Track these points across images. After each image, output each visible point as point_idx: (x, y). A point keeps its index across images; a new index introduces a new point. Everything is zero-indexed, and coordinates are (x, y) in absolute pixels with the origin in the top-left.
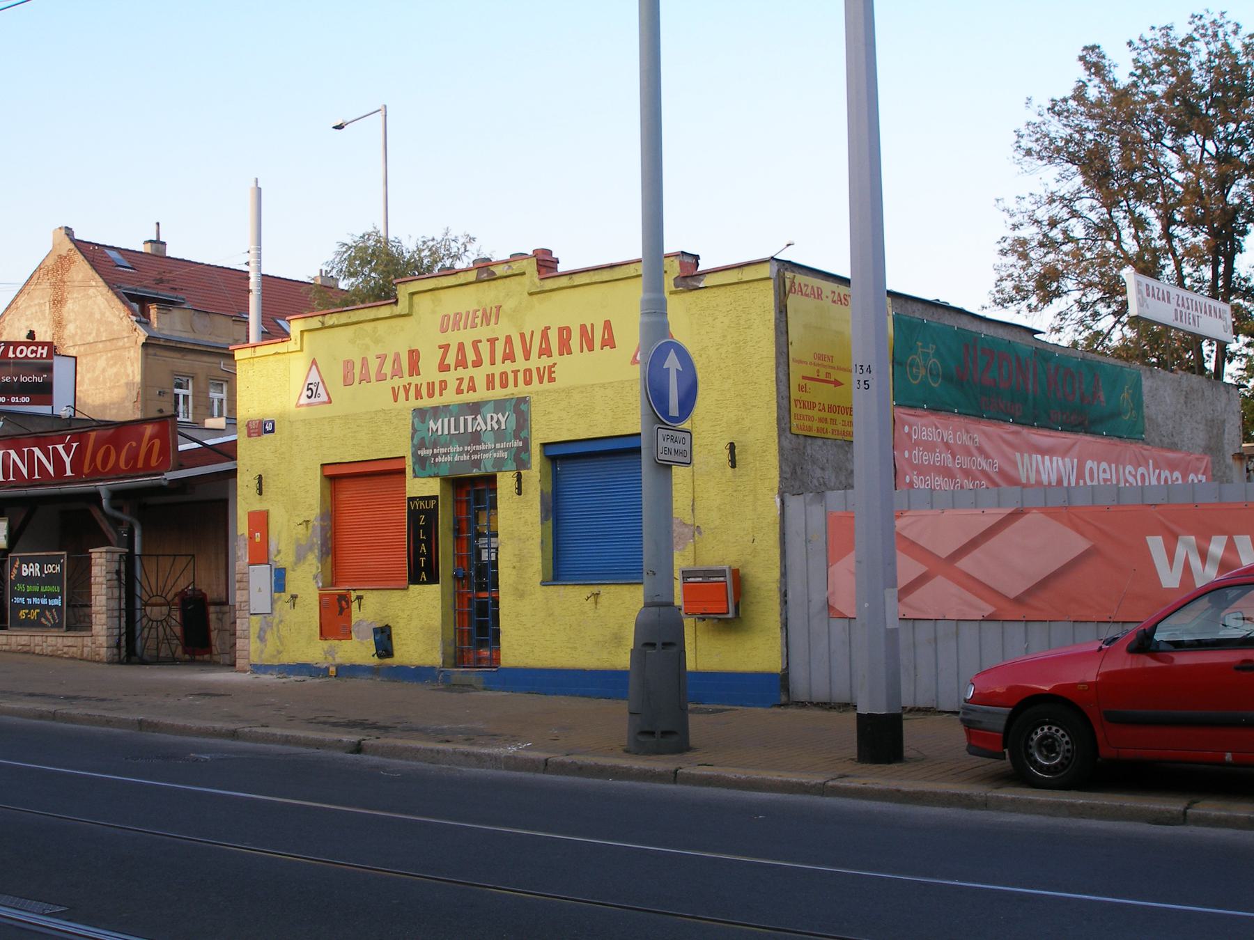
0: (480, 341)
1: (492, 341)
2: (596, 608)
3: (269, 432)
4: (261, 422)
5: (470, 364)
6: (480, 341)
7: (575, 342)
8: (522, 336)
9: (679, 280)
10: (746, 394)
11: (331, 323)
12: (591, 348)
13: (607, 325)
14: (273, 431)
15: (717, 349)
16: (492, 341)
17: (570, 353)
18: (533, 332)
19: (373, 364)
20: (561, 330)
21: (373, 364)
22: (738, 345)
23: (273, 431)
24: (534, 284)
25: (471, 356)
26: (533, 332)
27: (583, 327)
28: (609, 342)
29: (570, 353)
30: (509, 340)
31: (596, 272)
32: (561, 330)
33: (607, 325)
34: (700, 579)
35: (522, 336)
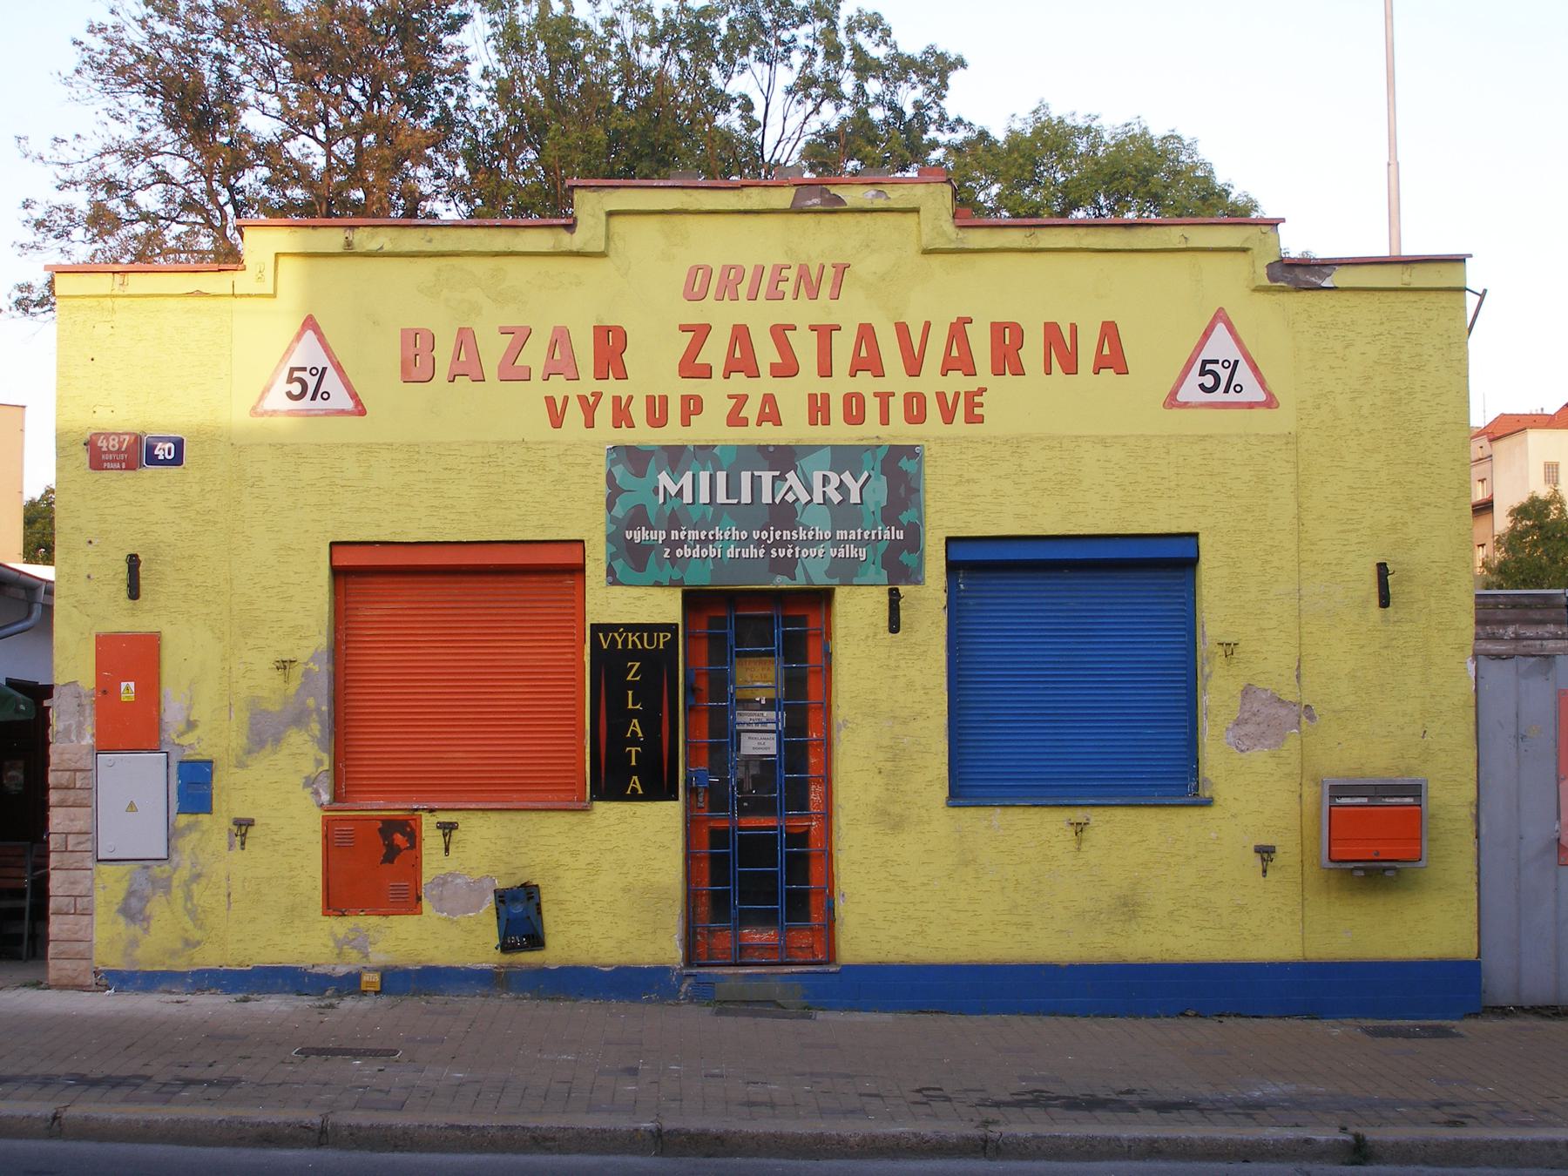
0: (794, 328)
1: (825, 333)
2: (1079, 849)
3: (165, 462)
4: (138, 439)
5: (764, 369)
6: (794, 328)
7: (1032, 352)
8: (902, 330)
9: (1278, 271)
10: (1411, 482)
11: (373, 246)
12: (1071, 368)
13: (1109, 331)
14: (178, 460)
15: (1353, 399)
16: (825, 333)
17: (1019, 371)
18: (927, 326)
19: (492, 350)
20: (998, 329)
21: (492, 350)
22: (1394, 396)
23: (178, 460)
24: (943, 234)
25: (766, 354)
26: (927, 326)
27: (1052, 330)
28: (1113, 359)
29: (1019, 371)
30: (866, 333)
31: (1091, 230)
32: (998, 329)
33: (1109, 331)
34: (1365, 800)
35: (902, 330)
